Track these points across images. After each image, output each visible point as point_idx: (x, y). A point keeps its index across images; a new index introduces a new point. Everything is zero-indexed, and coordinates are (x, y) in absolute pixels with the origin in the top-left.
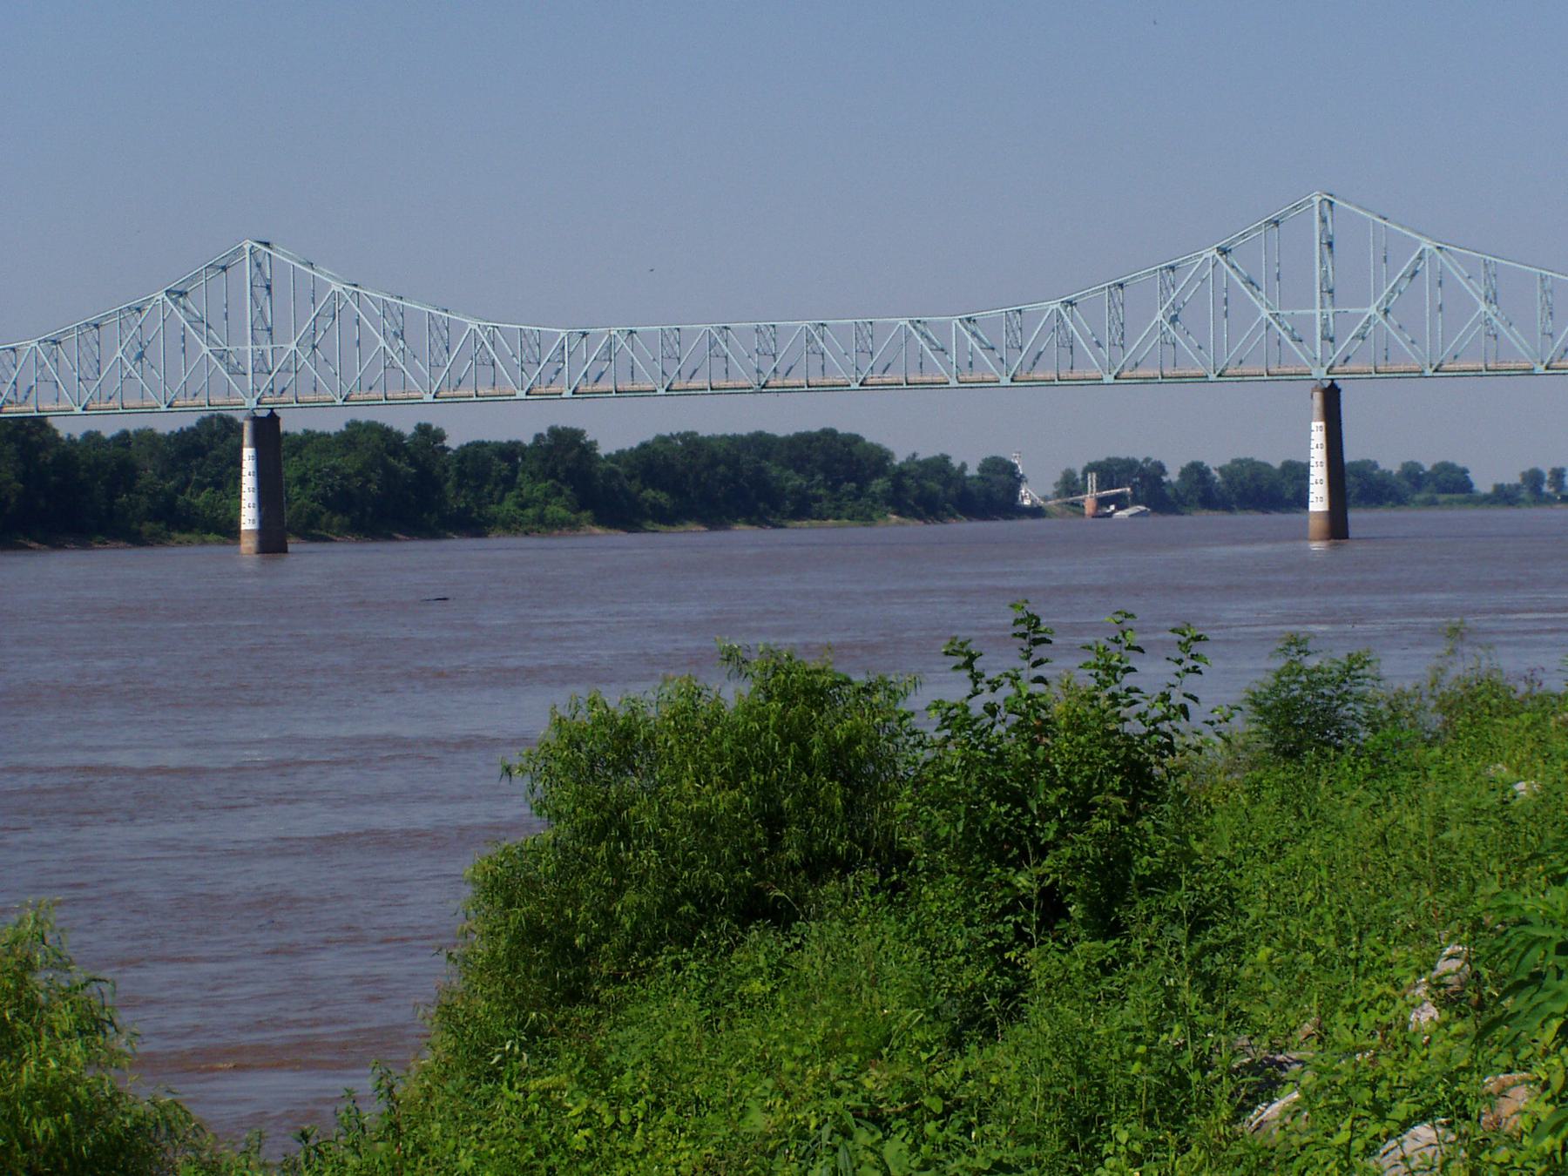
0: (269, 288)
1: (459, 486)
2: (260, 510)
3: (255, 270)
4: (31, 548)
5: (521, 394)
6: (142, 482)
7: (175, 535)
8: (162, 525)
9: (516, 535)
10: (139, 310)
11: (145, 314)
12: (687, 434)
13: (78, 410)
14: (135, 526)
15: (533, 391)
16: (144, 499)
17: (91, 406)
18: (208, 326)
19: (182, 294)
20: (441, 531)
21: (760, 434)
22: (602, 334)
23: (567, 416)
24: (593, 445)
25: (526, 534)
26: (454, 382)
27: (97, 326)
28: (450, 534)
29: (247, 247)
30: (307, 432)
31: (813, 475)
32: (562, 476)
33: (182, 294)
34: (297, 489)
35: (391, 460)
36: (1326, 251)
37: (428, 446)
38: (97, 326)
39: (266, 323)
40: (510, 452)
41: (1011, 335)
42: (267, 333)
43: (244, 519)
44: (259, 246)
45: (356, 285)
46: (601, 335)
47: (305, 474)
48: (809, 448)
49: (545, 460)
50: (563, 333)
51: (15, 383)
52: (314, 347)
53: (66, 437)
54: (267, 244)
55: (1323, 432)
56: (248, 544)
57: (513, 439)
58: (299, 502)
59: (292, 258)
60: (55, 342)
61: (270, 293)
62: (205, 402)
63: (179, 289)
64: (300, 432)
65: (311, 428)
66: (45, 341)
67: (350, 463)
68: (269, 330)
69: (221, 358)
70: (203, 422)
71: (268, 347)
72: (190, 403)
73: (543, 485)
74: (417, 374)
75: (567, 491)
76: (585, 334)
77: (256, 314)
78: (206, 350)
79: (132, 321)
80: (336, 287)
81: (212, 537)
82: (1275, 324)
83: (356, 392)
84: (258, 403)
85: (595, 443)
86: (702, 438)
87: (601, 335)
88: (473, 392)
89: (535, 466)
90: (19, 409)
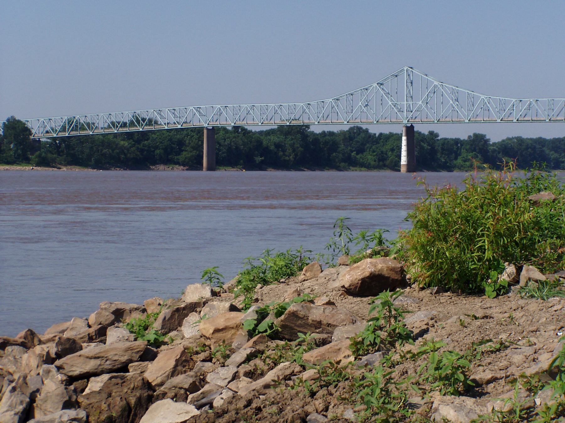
0: (412, 83)
1: (442, 153)
2: (408, 157)
3: (408, 77)
5: (499, 121)
7: (351, 167)
10: (367, 89)
12: (518, 137)
14: (338, 164)
15: (503, 120)
16: (341, 155)
17: (320, 122)
19: (382, 84)
20: (438, 169)
21: (540, 138)
22: (527, 101)
23: (480, 129)
24: (488, 140)
25: (466, 171)
27: (352, 95)
28: (441, 170)
29: (405, 69)
30: (391, 133)
31: (561, 154)
33: (382, 84)
36: (410, 84)
37: (433, 139)
38: (352, 95)
39: (410, 94)
40: (457, 141)
43: (402, 161)
46: (527, 101)
47: (393, 148)
48: (559, 144)
49: (472, 145)
50: (514, 100)
52: (427, 103)
54: (412, 68)
56: (403, 169)
58: (391, 158)
60: (337, 100)
61: (412, 85)
62: (219, 123)
63: (381, 82)
64: (388, 133)
67: (530, 142)
68: (412, 97)
69: (395, 106)
70: (351, 129)
71: (411, 103)
73: (471, 154)
74: (462, 113)
76: (521, 101)
77: (408, 91)
78: (390, 103)
80: (436, 83)
81: (363, 169)
82: (197, 114)
83: (441, 119)
84: (408, 122)
85: (489, 139)
86: (523, 138)
87: (527, 101)
90: (188, 125)
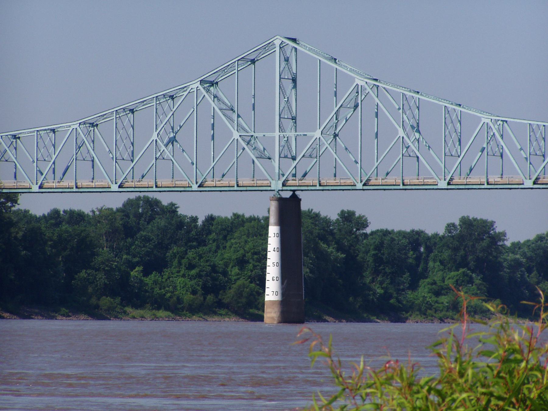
0: (294, 80)
3: (283, 64)
4: (377, 322)
6: (100, 259)
7: (129, 309)
8: (118, 300)
9: (432, 321)
11: (178, 102)
13: (115, 187)
14: (94, 301)
18: (239, 116)
24: (502, 236)
25: (442, 320)
26: (466, 170)
27: (132, 111)
29: (277, 43)
32: (472, 264)
34: (236, 270)
35: (324, 246)
37: (351, 232)
38: (132, 111)
41: (535, 143)
42: (291, 122)
44: (287, 42)
45: (376, 80)
47: (244, 256)
49: (456, 249)
51: (54, 163)
52: (336, 135)
53: (77, 210)
54: (294, 40)
55: (279, 238)
57: (416, 228)
58: (239, 283)
59: (317, 54)
60: (93, 125)
61: (295, 87)
64: (229, 215)
65: (240, 213)
66: (84, 123)
68: (294, 119)
70: (129, 203)
72: (218, 184)
75: (477, 280)
79: (166, 108)
80: (360, 81)
81: (161, 313)
88: (74, 184)
89: (446, 254)
